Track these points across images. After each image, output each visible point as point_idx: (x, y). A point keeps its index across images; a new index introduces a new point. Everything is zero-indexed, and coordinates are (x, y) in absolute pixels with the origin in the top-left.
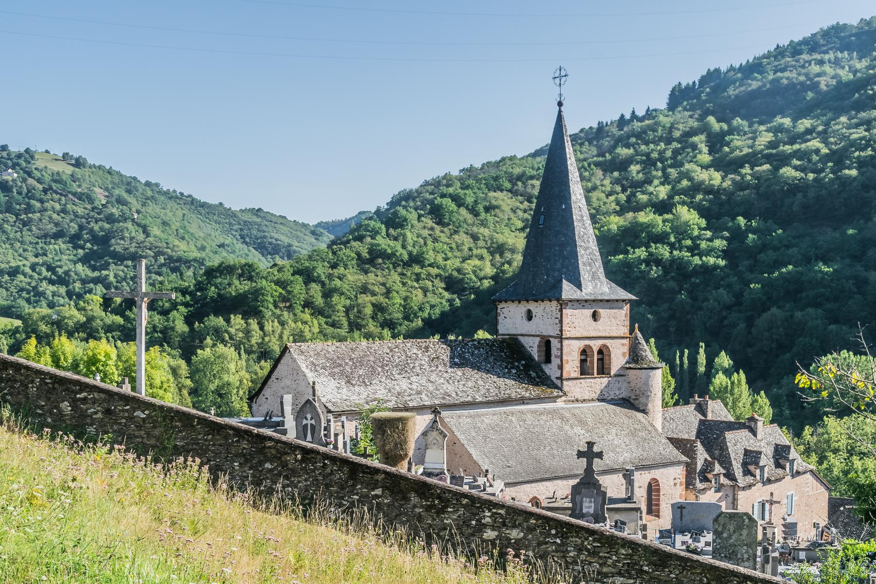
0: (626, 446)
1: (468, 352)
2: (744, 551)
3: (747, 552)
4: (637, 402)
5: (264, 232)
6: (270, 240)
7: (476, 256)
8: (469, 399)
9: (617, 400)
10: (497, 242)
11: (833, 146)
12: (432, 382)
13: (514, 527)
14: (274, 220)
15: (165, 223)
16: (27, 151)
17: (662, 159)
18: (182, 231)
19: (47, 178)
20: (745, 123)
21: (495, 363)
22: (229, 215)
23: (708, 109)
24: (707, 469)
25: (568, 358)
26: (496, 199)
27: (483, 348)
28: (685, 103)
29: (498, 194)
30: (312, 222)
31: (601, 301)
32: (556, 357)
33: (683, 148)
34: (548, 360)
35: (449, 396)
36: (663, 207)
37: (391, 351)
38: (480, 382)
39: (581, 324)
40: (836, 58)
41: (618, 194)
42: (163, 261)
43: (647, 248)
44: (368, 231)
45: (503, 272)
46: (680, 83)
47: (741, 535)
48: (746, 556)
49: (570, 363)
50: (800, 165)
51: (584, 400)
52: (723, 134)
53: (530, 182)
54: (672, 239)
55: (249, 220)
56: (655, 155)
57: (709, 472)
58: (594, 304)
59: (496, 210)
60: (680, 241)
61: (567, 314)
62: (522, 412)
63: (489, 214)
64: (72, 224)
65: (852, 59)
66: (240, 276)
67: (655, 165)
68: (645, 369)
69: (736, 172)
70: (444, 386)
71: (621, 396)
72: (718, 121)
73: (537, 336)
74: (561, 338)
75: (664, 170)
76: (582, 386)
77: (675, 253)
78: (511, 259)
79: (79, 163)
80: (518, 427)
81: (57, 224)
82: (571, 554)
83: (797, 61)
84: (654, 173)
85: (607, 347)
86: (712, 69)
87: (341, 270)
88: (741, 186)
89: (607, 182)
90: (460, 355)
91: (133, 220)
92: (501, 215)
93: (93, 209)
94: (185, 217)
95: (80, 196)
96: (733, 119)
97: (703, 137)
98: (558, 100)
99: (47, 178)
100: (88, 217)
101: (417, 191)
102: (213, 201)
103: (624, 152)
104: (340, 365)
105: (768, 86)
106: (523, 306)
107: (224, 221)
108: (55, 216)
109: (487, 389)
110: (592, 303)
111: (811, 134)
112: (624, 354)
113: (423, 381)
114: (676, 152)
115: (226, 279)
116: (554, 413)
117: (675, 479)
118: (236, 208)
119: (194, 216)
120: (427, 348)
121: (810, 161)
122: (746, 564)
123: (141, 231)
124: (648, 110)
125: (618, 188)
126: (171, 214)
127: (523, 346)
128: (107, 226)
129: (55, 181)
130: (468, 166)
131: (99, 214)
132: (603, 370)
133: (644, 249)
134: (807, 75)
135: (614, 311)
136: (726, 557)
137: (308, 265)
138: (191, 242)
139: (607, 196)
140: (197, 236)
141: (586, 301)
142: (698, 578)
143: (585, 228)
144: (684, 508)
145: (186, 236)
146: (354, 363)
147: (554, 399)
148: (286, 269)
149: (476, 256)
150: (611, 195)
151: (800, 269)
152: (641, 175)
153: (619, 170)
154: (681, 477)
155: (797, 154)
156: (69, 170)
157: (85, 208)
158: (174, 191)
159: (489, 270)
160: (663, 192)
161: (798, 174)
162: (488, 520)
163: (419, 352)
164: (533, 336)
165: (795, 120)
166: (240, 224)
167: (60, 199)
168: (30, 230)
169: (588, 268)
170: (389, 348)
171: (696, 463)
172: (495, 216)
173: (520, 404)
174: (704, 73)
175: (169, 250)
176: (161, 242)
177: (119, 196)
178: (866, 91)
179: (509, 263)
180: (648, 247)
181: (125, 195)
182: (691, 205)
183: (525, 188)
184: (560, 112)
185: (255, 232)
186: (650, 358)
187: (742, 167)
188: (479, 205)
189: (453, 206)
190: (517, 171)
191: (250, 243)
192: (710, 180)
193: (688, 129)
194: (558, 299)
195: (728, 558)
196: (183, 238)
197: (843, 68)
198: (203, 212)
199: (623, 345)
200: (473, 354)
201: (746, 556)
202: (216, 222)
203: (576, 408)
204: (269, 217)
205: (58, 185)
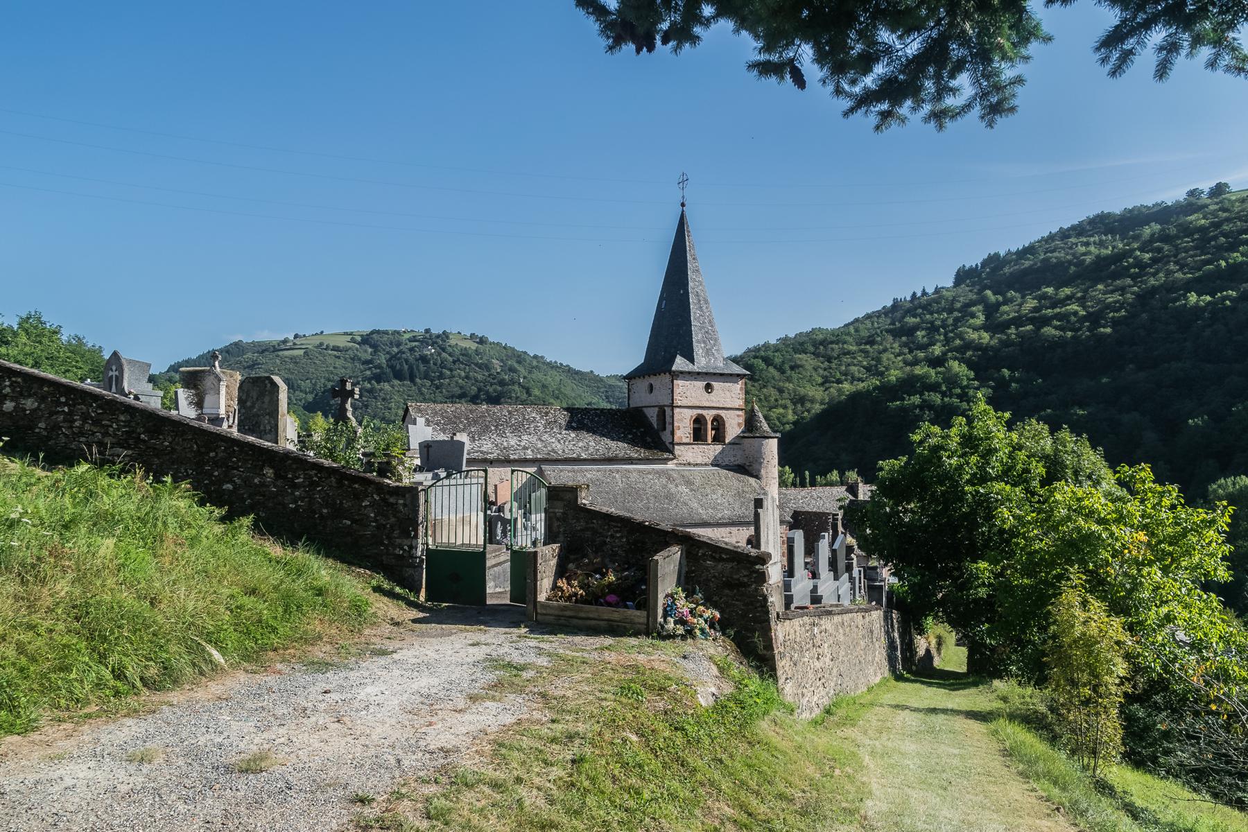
3: (269, 423)
7: (781, 406)
8: (575, 455)
10: (799, 395)
11: (1090, 309)
13: (30, 396)
15: (544, 386)
16: (444, 332)
17: (944, 326)
19: (457, 352)
20: (1018, 295)
21: (612, 429)
23: (986, 285)
28: (968, 281)
29: (802, 356)
31: (715, 374)
32: (670, 424)
33: (963, 317)
34: (664, 429)
35: (555, 452)
36: (936, 362)
40: (1101, 241)
41: (905, 355)
43: (921, 396)
45: (803, 418)
46: (964, 266)
47: (263, 403)
48: (268, 428)
50: (1060, 325)
52: (999, 304)
54: (944, 389)
56: (938, 323)
59: (800, 369)
60: (950, 390)
62: (627, 470)
64: (473, 387)
65: (1115, 240)
67: (937, 330)
68: (758, 437)
69: (1003, 332)
71: (736, 463)
72: (995, 294)
74: (672, 407)
75: (945, 335)
77: (946, 399)
79: (482, 341)
81: (461, 388)
82: (77, 424)
83: (1066, 244)
84: (937, 337)
85: (722, 417)
86: (992, 253)
88: (1006, 344)
89: (896, 345)
91: (519, 383)
92: (804, 373)
93: (490, 375)
95: (480, 366)
96: (1007, 292)
97: (980, 307)
99: (457, 352)
100: (485, 382)
101: (741, 356)
103: (911, 320)
105: (1039, 264)
108: (460, 381)
111: (1071, 300)
112: (739, 424)
114: (957, 320)
116: (659, 473)
119: (569, 381)
120: (547, 414)
121: (1068, 321)
123: (524, 391)
124: (936, 288)
125: (906, 350)
127: (646, 417)
128: (499, 388)
129: (463, 355)
131: (493, 379)
132: (719, 438)
133: (918, 396)
134: (1074, 255)
139: (896, 357)
141: (699, 373)
147: (665, 461)
149: (781, 406)
150: (899, 356)
151: (1058, 412)
152: (925, 339)
153: (907, 335)
155: (1058, 317)
156: (474, 346)
157: (484, 375)
158: (556, 362)
159: (791, 417)
160: (937, 350)
161: (1057, 333)
162: (8, 390)
164: (653, 406)
165: (1057, 289)
167: (465, 368)
168: (441, 392)
170: (509, 412)
174: (986, 257)
177: (511, 365)
178: (1121, 263)
179: (808, 411)
180: (921, 394)
181: (516, 365)
182: (961, 360)
184: (683, 211)
187: (1009, 328)
189: (762, 365)
190: (821, 337)
192: (979, 339)
193: (967, 301)
194: (670, 372)
196: (558, 398)
197: (1107, 248)
198: (577, 378)
199: (738, 416)
200: (592, 421)
201: (268, 428)
205: (465, 358)
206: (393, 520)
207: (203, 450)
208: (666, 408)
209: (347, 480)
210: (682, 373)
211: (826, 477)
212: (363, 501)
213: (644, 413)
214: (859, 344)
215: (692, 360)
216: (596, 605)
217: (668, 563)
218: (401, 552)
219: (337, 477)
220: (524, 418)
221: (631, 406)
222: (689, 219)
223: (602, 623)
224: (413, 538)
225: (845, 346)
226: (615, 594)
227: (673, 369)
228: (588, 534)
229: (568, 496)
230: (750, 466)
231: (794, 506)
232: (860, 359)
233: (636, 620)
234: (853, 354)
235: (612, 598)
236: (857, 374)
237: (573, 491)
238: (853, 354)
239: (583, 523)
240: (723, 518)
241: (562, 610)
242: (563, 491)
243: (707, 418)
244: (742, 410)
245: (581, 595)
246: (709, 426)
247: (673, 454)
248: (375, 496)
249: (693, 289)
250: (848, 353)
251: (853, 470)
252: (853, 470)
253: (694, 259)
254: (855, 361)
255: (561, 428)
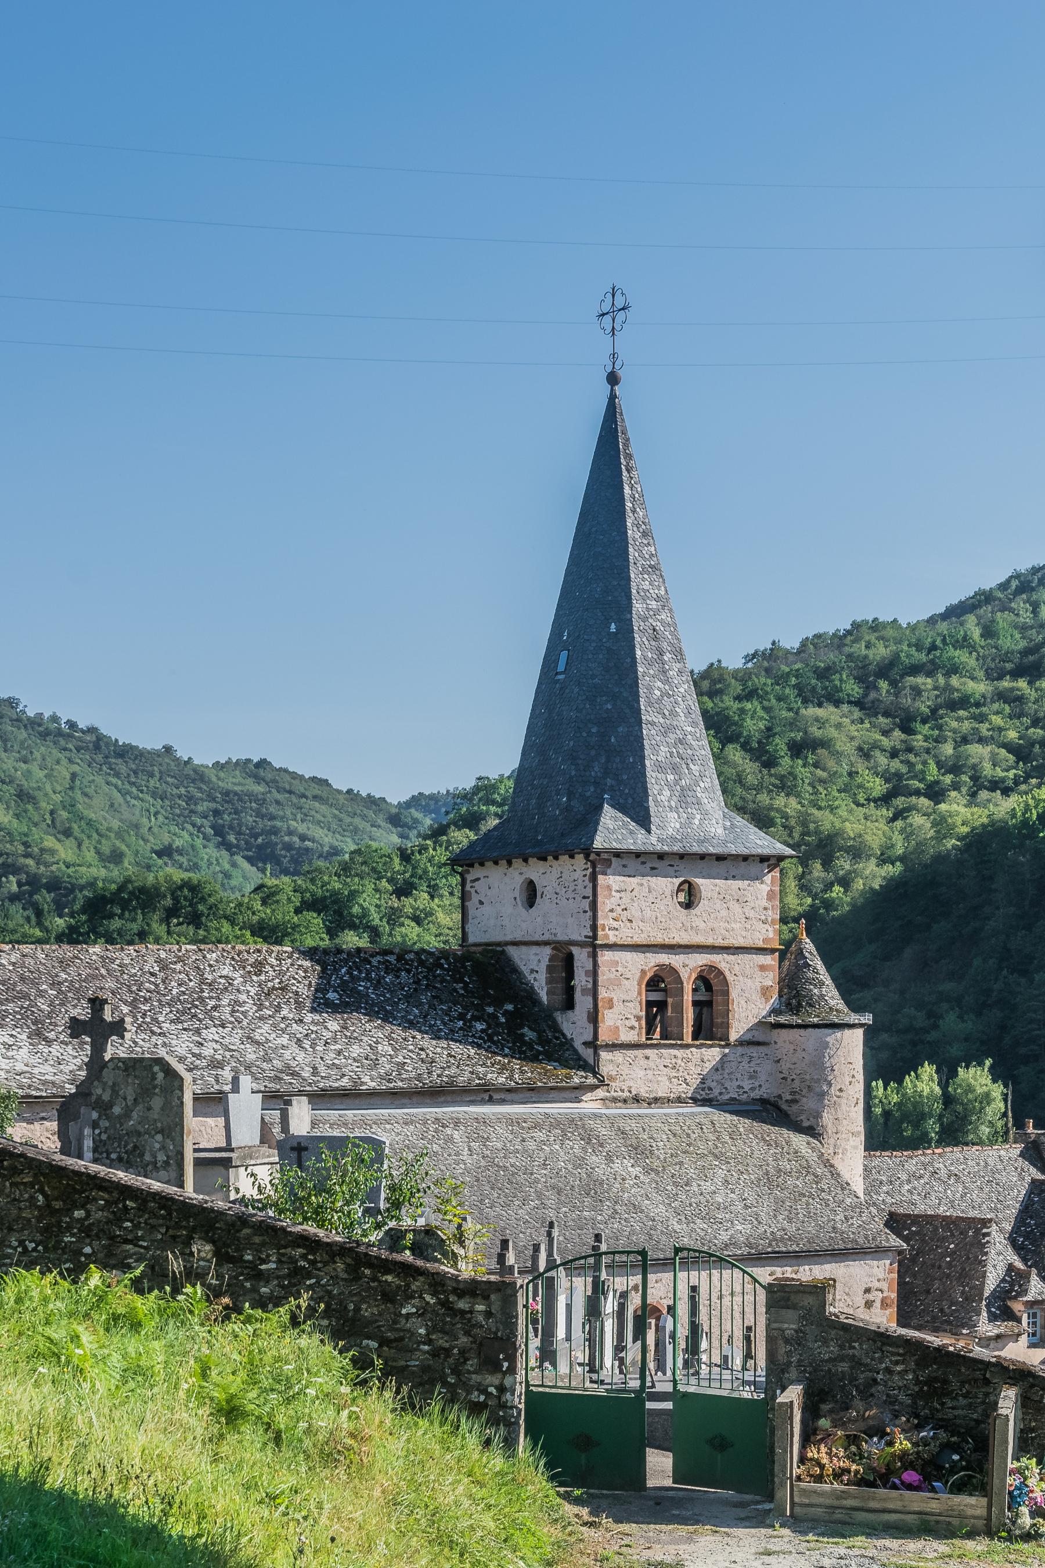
0: (746, 1207)
1: (368, 978)
2: (157, 1146)
3: (163, 1148)
4: (795, 1107)
5: (272, 818)
6: (287, 839)
8: (345, 1082)
9: (746, 1103)
10: (817, 832)
12: (258, 1043)
14: (300, 788)
18: (64, 814)
21: (432, 1007)
22: (187, 777)
24: (1012, 1290)
25: (613, 995)
26: (821, 723)
27: (408, 971)
29: (827, 712)
30: (396, 796)
31: (703, 857)
32: (584, 991)
34: (569, 1004)
35: (294, 1074)
37: (164, 968)
38: (385, 1048)
39: (648, 913)
42: (14, 888)
44: (493, 802)
45: (829, 905)
47: (149, 1109)
48: (161, 1157)
49: (618, 1007)
51: (656, 1100)
53: (910, 680)
55: (237, 788)
57: (1015, 1298)
58: (681, 865)
61: (609, 888)
62: (483, 1121)
63: (800, 762)
66: (171, 913)
70: (287, 1055)
71: (756, 1094)
73: (546, 943)
74: (593, 946)
76: (651, 1064)
78: (849, 872)
80: (466, 1152)
85: (720, 973)
87: (422, 899)
90: (344, 983)
92: (831, 764)
94: (78, 783)
98: (609, 369)
102: (148, 741)
104: (26, 996)
106: (516, 874)
107: (175, 791)
109: (398, 1064)
110: (676, 862)
112: (765, 991)
113: (234, 1040)
115: (134, 920)
117: (868, 1291)
118: (204, 758)
119: (99, 780)
120: (259, 967)
122: (162, 1173)
126: (41, 774)
127: (515, 970)
130: (764, 645)
135: (739, 883)
136: (120, 1159)
137: (338, 886)
138: (86, 841)
140: (102, 829)
141: (661, 856)
142: (26, 1196)
143: (667, 681)
144: (306, 1149)
145: (75, 826)
146: (60, 992)
147: (576, 1092)
148: (283, 897)
154: (885, 1286)
158: (55, 719)
163: (237, 975)
164: (537, 943)
166: (214, 800)
169: (671, 777)
170: (159, 961)
171: (984, 1275)
172: (816, 765)
173: (483, 1102)
175: (30, 862)
176: (11, 842)
179: (845, 882)
183: (897, 695)
184: (613, 397)
185: (249, 819)
186: (832, 1003)
188: (777, 740)
190: (881, 652)
191: (237, 846)
194: (587, 852)
195: (125, 1164)
196: (67, 833)
198: (123, 769)
199: (763, 968)
200: (378, 984)
201: (161, 1157)
202: (154, 795)
203: (630, 1117)
204: (285, 782)
206: (463, 1340)
207: (57, 1205)
208: (575, 950)
209: (370, 1266)
210: (618, 854)
211: (900, 1082)
212: (402, 1306)
213: (509, 960)
214: (994, 675)
215: (643, 820)
216: (885, 1487)
217: (1008, 1402)
218: (482, 1398)
219: (349, 1260)
220: (203, 981)
221: (472, 939)
222: (630, 421)
223: (909, 1518)
224: (505, 1373)
225: (955, 681)
226: (914, 1470)
227: (598, 843)
228: (844, 1367)
229: (809, 1300)
230: (795, 1101)
231: (889, 1200)
232: (997, 720)
233: (970, 1512)
234: (978, 705)
235: (911, 1476)
236: (988, 770)
237: (820, 1290)
238: (978, 705)
239: (833, 1348)
240: (731, 1243)
241: (838, 1498)
242: (799, 1292)
243: (684, 974)
244: (773, 951)
245: (857, 1472)
246: (688, 997)
247: (595, 1073)
248: (428, 1298)
249: (645, 619)
250: (963, 702)
251: (981, 1064)
252: (981, 1064)
253: (645, 534)
254: (984, 728)
255: (299, 1005)
